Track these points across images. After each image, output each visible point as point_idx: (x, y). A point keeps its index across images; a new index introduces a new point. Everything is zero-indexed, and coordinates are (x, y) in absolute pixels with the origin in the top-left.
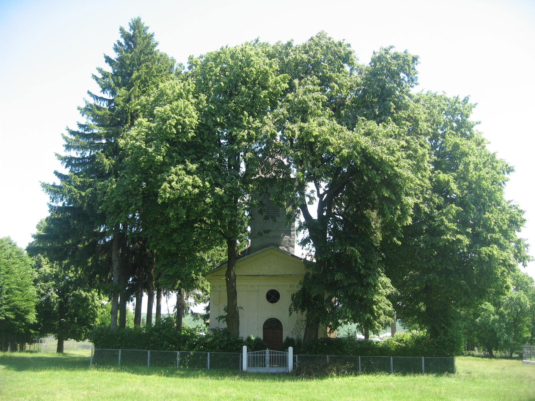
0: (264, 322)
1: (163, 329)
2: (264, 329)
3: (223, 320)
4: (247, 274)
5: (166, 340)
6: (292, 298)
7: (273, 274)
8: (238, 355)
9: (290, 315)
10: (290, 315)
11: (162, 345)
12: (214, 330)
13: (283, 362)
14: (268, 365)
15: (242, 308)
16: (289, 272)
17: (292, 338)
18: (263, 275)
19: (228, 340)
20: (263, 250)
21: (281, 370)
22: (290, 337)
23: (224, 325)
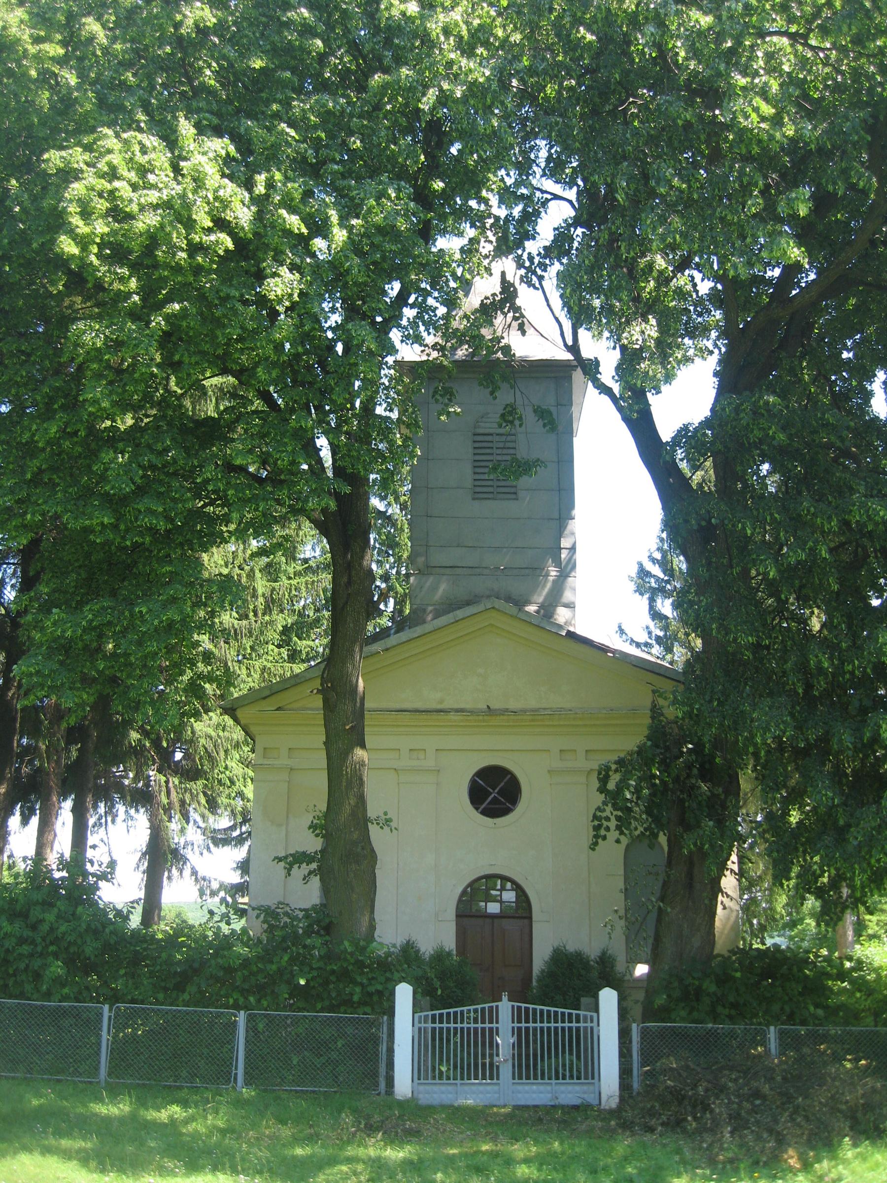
1: (47, 904)
2: (459, 916)
3: (305, 869)
5: (56, 956)
9: (593, 846)
10: (593, 846)
11: (37, 976)
12: (269, 914)
16: (556, 701)
18: (458, 711)
19: (328, 957)
20: (460, 614)
21: (569, 1093)
23: (306, 894)
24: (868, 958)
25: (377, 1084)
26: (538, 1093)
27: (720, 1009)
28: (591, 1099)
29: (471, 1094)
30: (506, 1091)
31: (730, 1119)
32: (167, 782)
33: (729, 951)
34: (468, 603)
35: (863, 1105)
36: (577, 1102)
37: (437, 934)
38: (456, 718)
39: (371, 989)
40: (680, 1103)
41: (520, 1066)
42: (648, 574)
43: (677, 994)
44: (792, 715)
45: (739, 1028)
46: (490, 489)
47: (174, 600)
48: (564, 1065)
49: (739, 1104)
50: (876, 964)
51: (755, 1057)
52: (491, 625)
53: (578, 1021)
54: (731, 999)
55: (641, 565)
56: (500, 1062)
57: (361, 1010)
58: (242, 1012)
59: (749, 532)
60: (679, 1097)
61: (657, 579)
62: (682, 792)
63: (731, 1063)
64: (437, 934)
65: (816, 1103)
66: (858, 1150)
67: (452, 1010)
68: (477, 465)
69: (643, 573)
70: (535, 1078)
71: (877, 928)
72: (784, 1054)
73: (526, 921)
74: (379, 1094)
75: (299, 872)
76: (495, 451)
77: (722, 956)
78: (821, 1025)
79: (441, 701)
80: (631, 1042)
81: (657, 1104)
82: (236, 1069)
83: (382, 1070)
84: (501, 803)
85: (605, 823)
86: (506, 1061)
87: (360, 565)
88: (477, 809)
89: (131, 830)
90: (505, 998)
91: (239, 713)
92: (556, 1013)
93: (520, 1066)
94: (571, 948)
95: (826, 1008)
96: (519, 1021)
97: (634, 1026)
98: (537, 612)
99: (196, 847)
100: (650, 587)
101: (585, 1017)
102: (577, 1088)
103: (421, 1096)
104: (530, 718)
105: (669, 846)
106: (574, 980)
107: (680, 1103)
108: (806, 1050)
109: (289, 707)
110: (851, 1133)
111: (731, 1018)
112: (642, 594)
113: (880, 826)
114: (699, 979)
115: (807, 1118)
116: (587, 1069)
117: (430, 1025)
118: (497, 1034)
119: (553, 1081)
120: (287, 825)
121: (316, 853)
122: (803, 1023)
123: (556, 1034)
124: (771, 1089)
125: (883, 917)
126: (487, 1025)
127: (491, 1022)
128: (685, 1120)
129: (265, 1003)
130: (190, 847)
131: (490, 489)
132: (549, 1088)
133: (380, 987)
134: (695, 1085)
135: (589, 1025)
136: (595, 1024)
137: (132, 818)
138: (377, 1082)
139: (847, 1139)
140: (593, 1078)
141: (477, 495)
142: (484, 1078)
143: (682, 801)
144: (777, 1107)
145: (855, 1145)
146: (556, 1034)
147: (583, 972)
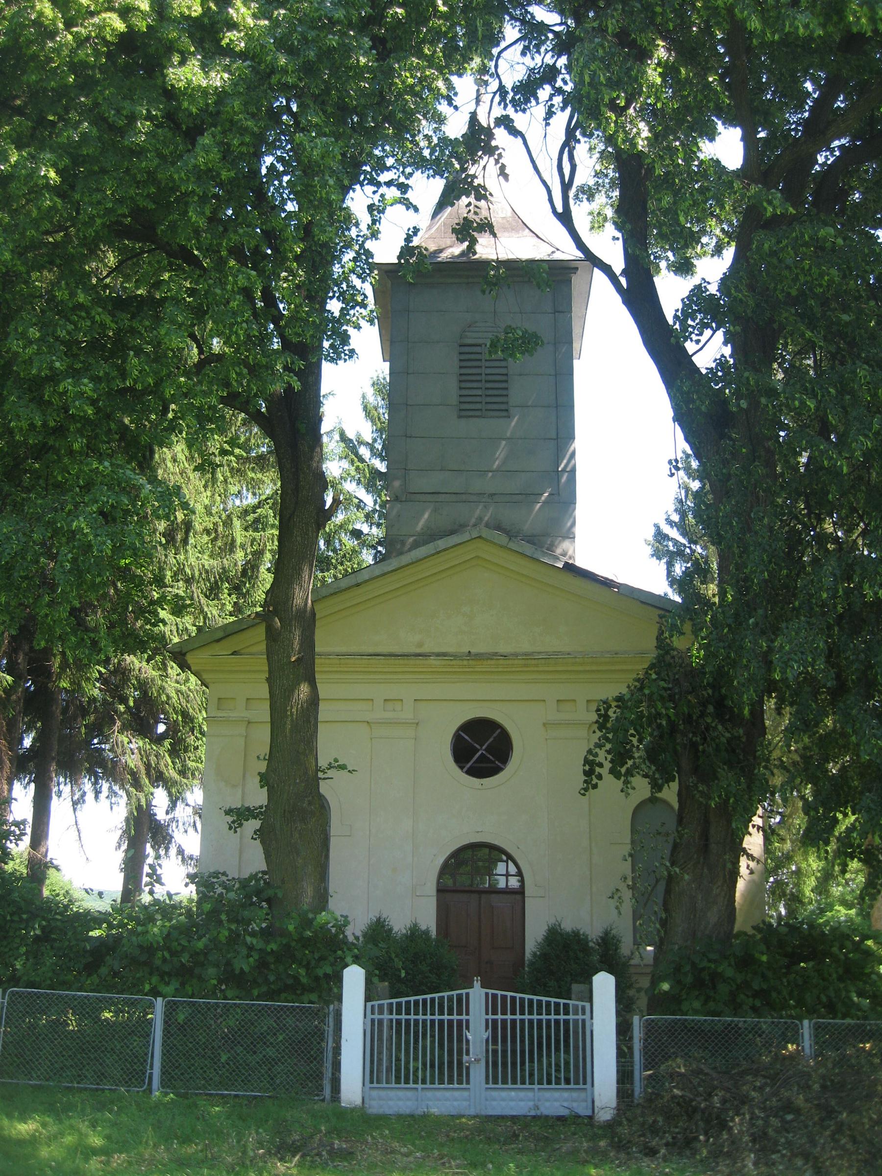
0: (441, 860)
2: (441, 891)
4: (371, 650)
6: (602, 722)
8: (316, 1014)
15: (343, 767)
17: (576, 934)
18: (438, 655)
20: (441, 544)
22: (568, 926)
25: (320, 1088)
26: (514, 1101)
28: (583, 1110)
29: (440, 1101)
30: (478, 1096)
31: (754, 1141)
33: (753, 928)
34: (452, 532)
36: (564, 1112)
37: (414, 909)
38: (438, 663)
40: (690, 1117)
41: (495, 1064)
42: (666, 537)
43: (689, 979)
45: (765, 1023)
46: (478, 406)
48: (549, 1065)
49: (766, 1120)
51: (784, 1058)
52: (477, 557)
53: (567, 1013)
54: (756, 986)
55: (657, 527)
56: (470, 1062)
57: (305, 998)
58: (160, 999)
60: (689, 1109)
61: (676, 542)
63: (755, 1067)
64: (414, 909)
65: (866, 1120)
68: (463, 379)
69: (660, 536)
70: (514, 1082)
72: (821, 1054)
73: (518, 897)
74: (323, 1100)
76: (483, 363)
77: (745, 934)
78: (866, 1018)
79: (420, 645)
80: (631, 1038)
81: (660, 1119)
82: (152, 1068)
83: (328, 1074)
85: (598, 769)
86: (477, 1061)
87: (309, 467)
88: (462, 768)
89: (114, 807)
90: (477, 984)
91: (190, 659)
93: (495, 1064)
96: (495, 1012)
97: (636, 1019)
99: (180, 824)
100: (668, 551)
101: (576, 1008)
102: (566, 1094)
103: (374, 1103)
104: (523, 662)
105: (680, 801)
107: (690, 1117)
109: (247, 650)
111: (755, 1010)
112: (659, 558)
114: (715, 961)
115: (854, 1140)
116: (578, 1073)
117: (386, 1016)
118: (468, 1028)
119: (536, 1086)
120: (244, 786)
123: (504, 1028)
124: (806, 1100)
127: (460, 1013)
128: (696, 1139)
129: (189, 990)
131: (478, 406)
134: (710, 1095)
136: (587, 1016)
137: (116, 794)
138: (321, 1085)
140: (585, 1083)
141: (463, 413)
142: (451, 1082)
143: (694, 745)
144: (815, 1124)
146: (504, 1028)
147: (581, 955)
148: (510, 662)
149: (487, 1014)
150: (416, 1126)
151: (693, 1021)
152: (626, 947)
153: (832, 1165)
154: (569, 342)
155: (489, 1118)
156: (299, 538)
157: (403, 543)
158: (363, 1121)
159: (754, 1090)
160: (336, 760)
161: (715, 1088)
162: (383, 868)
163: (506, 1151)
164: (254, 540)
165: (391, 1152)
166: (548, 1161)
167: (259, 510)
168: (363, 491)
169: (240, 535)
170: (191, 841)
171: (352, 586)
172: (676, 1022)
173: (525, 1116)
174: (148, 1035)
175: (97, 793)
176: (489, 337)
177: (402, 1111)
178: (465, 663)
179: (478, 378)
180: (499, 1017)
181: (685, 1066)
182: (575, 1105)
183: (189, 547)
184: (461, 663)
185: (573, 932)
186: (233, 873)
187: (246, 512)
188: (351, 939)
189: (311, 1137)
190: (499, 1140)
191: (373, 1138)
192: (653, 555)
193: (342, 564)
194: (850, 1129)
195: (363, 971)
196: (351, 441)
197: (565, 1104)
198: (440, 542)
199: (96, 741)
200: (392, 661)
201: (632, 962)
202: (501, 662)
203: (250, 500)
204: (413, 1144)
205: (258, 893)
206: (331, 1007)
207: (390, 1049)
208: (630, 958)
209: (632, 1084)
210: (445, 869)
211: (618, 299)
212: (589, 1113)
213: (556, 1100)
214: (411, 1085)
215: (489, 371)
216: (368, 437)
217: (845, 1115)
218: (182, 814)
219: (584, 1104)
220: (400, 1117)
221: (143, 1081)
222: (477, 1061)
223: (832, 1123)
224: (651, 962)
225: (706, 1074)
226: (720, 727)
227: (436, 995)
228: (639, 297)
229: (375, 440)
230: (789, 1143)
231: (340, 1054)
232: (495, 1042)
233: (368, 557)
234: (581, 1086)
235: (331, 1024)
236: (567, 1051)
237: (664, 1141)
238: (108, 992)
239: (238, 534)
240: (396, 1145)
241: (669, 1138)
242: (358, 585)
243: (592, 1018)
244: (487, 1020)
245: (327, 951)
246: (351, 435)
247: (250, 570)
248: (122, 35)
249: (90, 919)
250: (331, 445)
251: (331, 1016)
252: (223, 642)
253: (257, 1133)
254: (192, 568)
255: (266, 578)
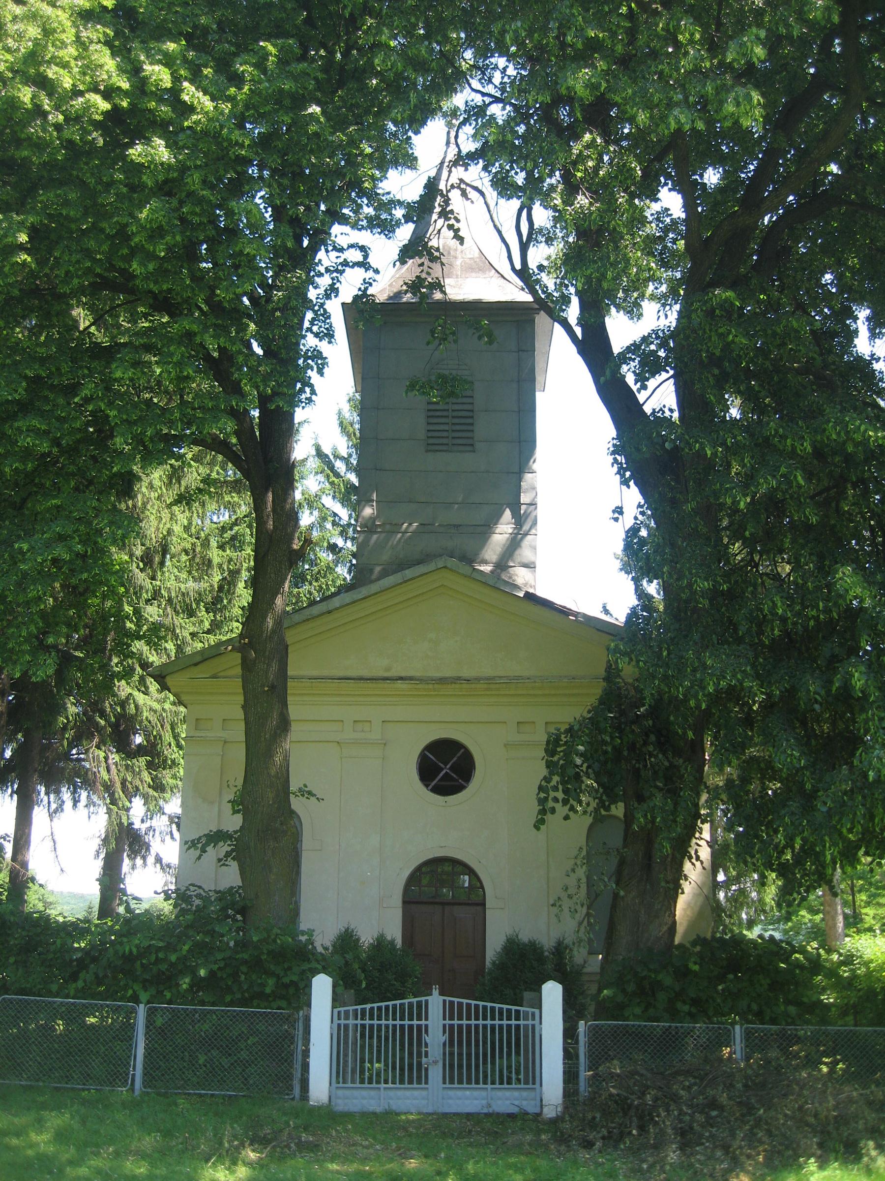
0: (407, 873)
2: (405, 902)
3: (224, 847)
4: (341, 674)
7: (448, 673)
10: (539, 824)
13: (514, 1056)
14: (436, 1073)
20: (409, 573)
24: (858, 951)
25: (291, 1088)
26: (470, 1099)
27: (679, 1005)
29: (409, 1100)
30: (435, 1095)
32: (106, 758)
34: (419, 562)
35: (836, 1117)
36: (515, 1110)
37: (380, 920)
39: (286, 980)
40: (625, 1114)
41: (452, 1066)
43: (631, 987)
44: (753, 666)
46: (445, 441)
47: (62, 538)
48: (509, 1067)
49: (692, 1116)
50: (866, 957)
59: (709, 453)
60: (624, 1106)
62: (638, 761)
64: (380, 920)
65: (780, 1116)
66: (826, 1173)
67: (390, 1003)
71: (873, 922)
73: (479, 908)
75: (213, 853)
79: (388, 669)
80: (577, 1042)
82: (134, 1069)
83: (297, 1075)
84: (453, 779)
88: (427, 786)
89: (93, 816)
90: (435, 992)
91: (169, 681)
92: (501, 1010)
93: (452, 1066)
94: (525, 937)
95: (798, 1004)
98: (492, 572)
99: (157, 833)
101: (526, 1014)
102: (516, 1094)
103: (340, 1101)
106: (523, 969)
108: (773, 1054)
109: (222, 674)
110: (819, 1152)
112: (627, 573)
113: (852, 790)
115: (769, 1133)
116: (528, 1074)
117: (351, 1022)
119: (489, 1086)
121: (236, 832)
122: (773, 1021)
124: (730, 1098)
125: (881, 911)
126: (415, 1022)
130: (151, 833)
132: (484, 1093)
133: (295, 978)
134: (644, 1094)
135: (530, 1022)
136: (537, 1022)
138: (291, 1085)
139: (812, 1160)
140: (534, 1083)
144: (736, 1119)
145: (821, 1167)
146: (477, 1032)
148: (473, 686)
149: (444, 1019)
150: (383, 1126)
151: (633, 1026)
152: (579, 955)
153: (741, 1154)
154: (533, 380)
155: (445, 1115)
156: (273, 575)
157: (371, 571)
158: (330, 1116)
159: (683, 1089)
160: (305, 786)
161: (648, 1087)
162: (350, 890)
163: (459, 1144)
164: (230, 560)
165: (353, 1145)
166: (496, 1152)
167: (236, 528)
168: (339, 505)
169: (215, 555)
170: (168, 848)
171: (323, 614)
172: (618, 1027)
173: (479, 1114)
174: (131, 1039)
175: (76, 802)
176: (450, 381)
177: (365, 1110)
178: (431, 686)
179: (445, 413)
180: (456, 1022)
181: (621, 1068)
182: (524, 1103)
183: (165, 569)
184: (426, 686)
185: (530, 941)
186: (209, 886)
187: (223, 529)
188: (320, 949)
189: (281, 1131)
190: (453, 1135)
191: (336, 1130)
192: (621, 570)
193: (317, 580)
194: (767, 1123)
195: (330, 980)
196: (327, 456)
197: (516, 1103)
198: (407, 572)
199: (74, 751)
200: (362, 684)
201: (585, 970)
202: (465, 686)
203: (225, 517)
204: (374, 1138)
205: (232, 905)
206: (301, 1013)
207: (354, 1052)
208: (583, 967)
209: (578, 1084)
210: (414, 878)
211: (573, 349)
212: (537, 1110)
213: (507, 1099)
214: (374, 1085)
215: (456, 407)
216: (344, 452)
217: (762, 1111)
218: (159, 824)
219: (533, 1102)
220: (364, 1114)
221: (126, 1081)
222: (435, 1062)
223: (752, 1118)
224: (598, 970)
225: (642, 1075)
226: (660, 756)
227: (398, 1002)
228: (594, 346)
229: (350, 455)
230: (712, 1136)
231: (308, 1056)
232: (451, 1044)
233: (342, 571)
234: (531, 1086)
235: (301, 1029)
236: (518, 1053)
237: (600, 1135)
238: (93, 999)
239: (215, 553)
240: (358, 1138)
241: (604, 1132)
242: (329, 612)
243: (541, 1023)
244: (444, 1026)
245: (301, 961)
246: (327, 450)
247: (227, 585)
248: (106, 114)
249: (74, 929)
250: (301, 449)
251: (301, 1021)
252: (200, 666)
253: (233, 1128)
254: (169, 590)
255: (243, 595)
